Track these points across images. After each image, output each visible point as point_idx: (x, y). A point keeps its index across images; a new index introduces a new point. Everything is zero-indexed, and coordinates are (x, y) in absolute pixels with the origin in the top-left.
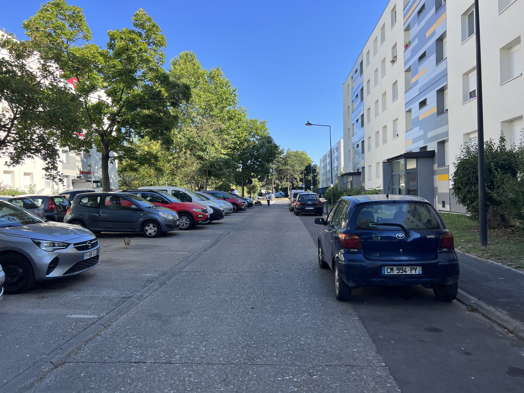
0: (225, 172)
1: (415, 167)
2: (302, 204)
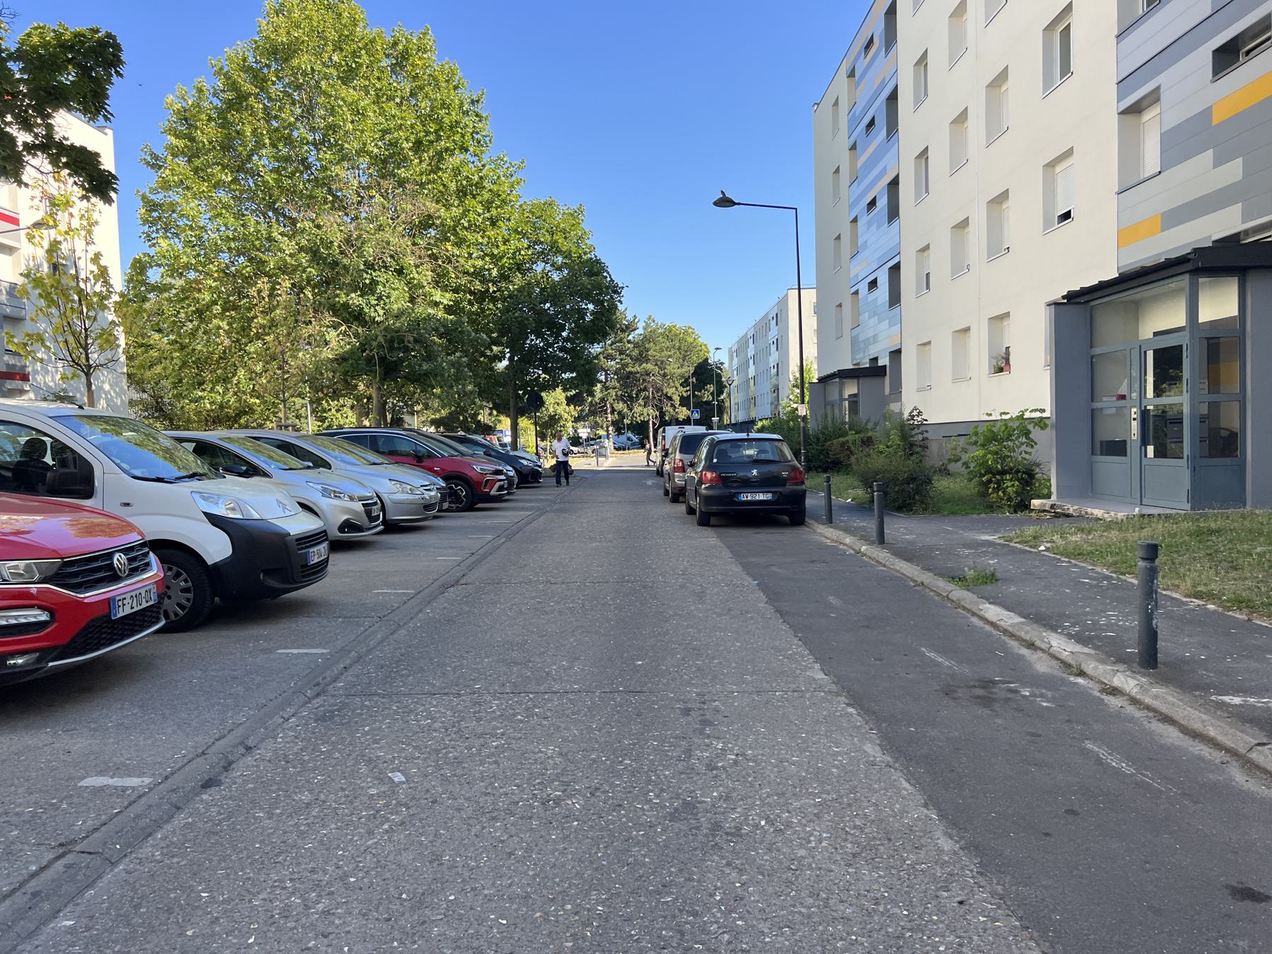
0: (441, 365)
1: (856, 392)
2: (723, 481)
